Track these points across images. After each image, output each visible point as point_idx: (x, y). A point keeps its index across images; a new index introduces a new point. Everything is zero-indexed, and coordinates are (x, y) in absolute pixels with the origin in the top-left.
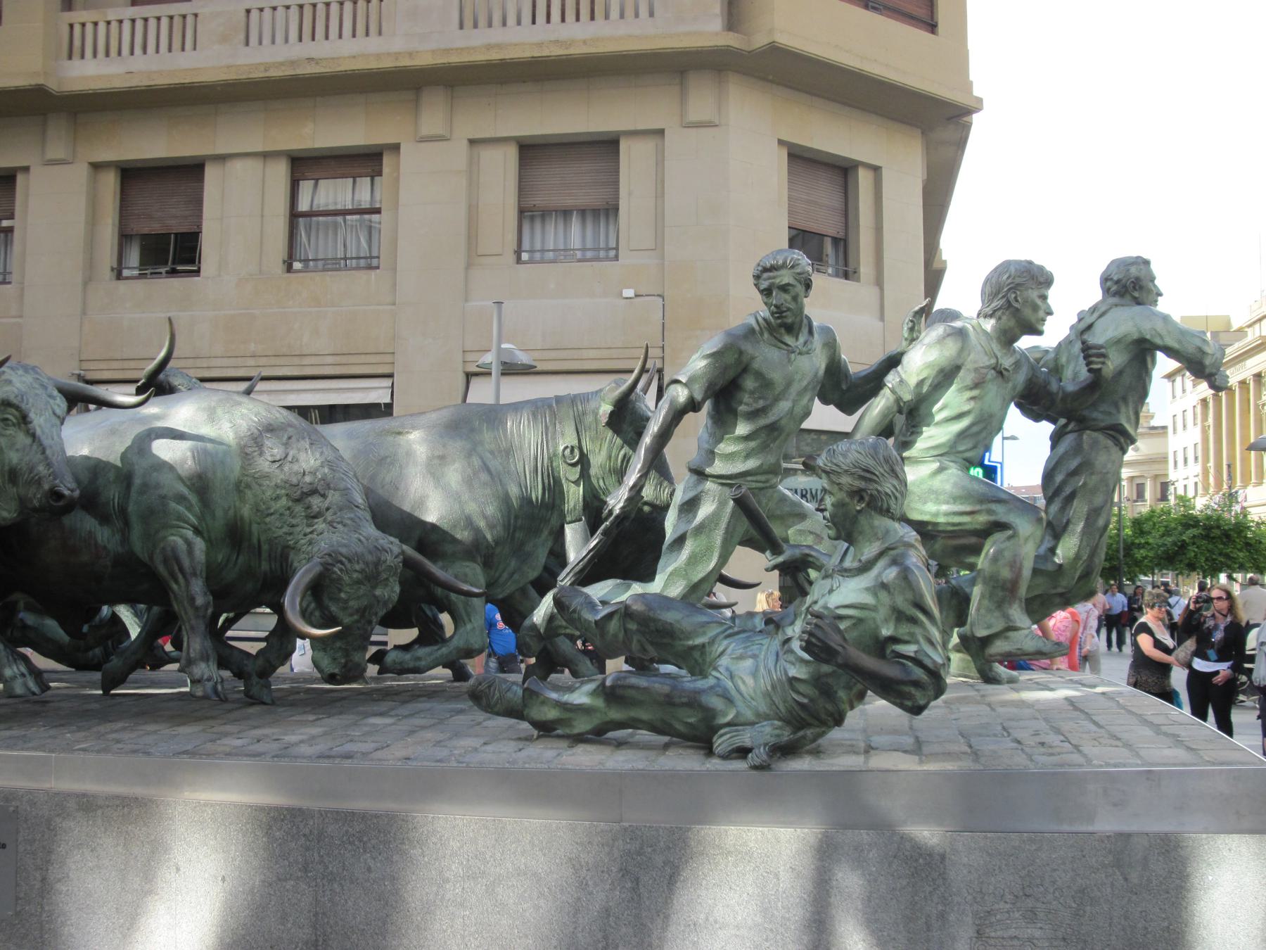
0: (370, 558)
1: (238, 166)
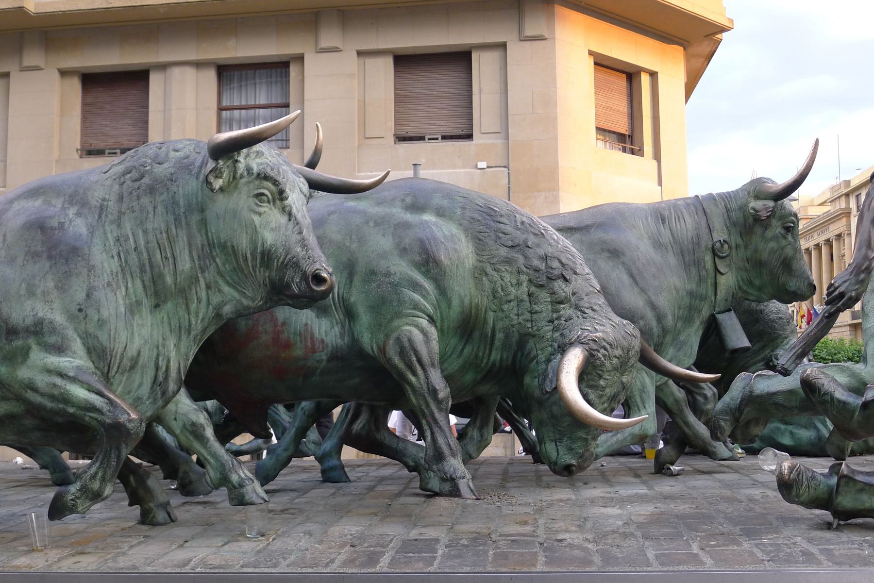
0: (625, 343)
1: (176, 71)
